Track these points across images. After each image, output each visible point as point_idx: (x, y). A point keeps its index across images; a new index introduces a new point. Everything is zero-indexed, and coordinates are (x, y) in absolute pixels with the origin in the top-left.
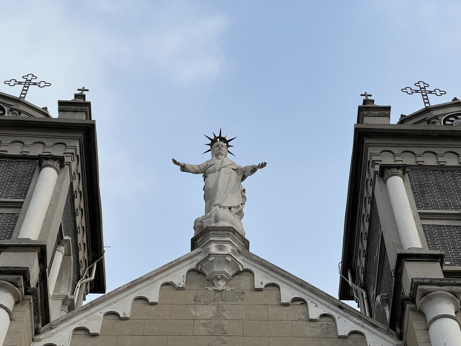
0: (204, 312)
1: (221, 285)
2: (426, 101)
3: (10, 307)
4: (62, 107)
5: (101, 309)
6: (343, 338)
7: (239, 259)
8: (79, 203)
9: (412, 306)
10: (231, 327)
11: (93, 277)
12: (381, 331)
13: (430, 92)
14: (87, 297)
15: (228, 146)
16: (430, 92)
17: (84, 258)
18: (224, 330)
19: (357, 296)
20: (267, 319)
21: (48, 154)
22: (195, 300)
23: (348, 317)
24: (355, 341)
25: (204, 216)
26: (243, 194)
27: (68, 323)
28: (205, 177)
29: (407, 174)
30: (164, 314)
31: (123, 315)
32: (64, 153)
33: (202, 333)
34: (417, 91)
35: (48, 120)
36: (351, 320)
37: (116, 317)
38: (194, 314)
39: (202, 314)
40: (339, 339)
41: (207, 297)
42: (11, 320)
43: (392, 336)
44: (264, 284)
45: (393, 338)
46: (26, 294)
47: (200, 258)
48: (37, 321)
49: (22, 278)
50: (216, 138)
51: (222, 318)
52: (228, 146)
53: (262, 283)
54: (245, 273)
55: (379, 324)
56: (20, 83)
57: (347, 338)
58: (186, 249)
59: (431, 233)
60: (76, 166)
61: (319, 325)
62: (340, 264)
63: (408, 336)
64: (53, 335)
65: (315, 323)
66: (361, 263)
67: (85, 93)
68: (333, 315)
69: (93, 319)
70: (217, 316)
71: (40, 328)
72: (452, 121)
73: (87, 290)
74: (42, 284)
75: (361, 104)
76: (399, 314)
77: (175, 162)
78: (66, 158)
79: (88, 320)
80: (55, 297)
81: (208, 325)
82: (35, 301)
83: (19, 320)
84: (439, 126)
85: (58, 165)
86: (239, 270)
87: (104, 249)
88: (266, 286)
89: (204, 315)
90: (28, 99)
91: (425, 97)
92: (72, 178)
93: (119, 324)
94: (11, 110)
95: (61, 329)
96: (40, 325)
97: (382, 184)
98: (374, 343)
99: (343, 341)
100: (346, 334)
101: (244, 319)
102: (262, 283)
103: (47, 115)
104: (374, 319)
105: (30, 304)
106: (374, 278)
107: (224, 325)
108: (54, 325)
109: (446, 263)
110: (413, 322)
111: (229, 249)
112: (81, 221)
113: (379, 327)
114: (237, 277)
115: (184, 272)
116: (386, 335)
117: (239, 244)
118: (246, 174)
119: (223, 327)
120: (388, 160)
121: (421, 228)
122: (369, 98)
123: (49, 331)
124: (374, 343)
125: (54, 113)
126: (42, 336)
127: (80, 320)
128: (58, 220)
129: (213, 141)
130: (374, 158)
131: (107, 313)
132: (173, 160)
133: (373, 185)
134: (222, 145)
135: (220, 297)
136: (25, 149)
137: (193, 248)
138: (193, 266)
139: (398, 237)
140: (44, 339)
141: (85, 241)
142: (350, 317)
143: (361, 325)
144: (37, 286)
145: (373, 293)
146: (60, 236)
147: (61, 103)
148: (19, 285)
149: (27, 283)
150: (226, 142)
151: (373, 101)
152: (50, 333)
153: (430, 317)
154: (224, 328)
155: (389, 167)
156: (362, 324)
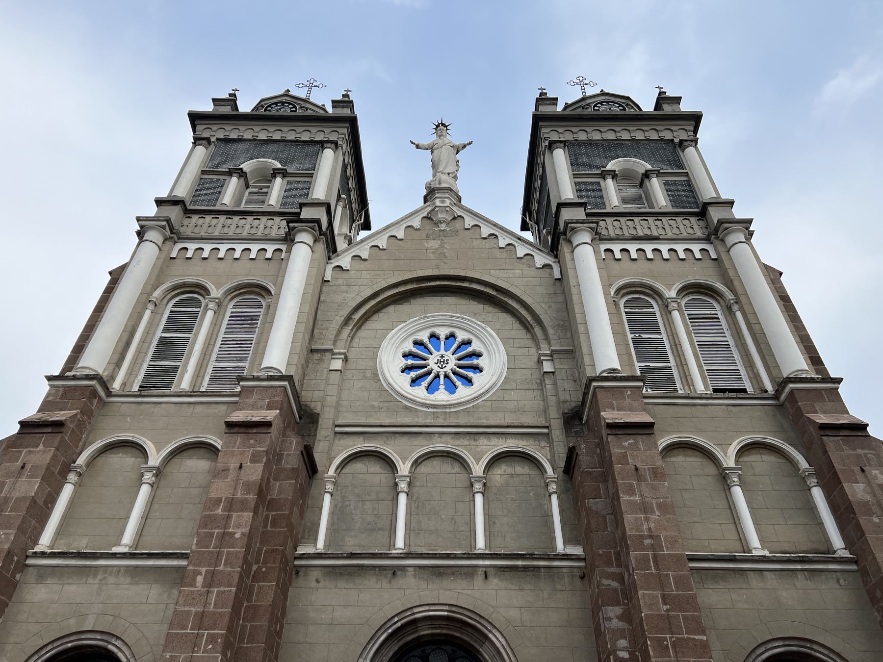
1: (443, 227)
2: (583, 91)
3: (311, 244)
4: (335, 104)
5: (368, 243)
7: (455, 209)
9: (564, 237)
11: (362, 221)
13: (586, 84)
14: (359, 233)
15: (447, 129)
16: (586, 84)
17: (356, 208)
19: (532, 229)
21: (327, 139)
22: (426, 237)
25: (432, 180)
26: (457, 163)
28: (432, 152)
29: (566, 147)
32: (338, 138)
34: (577, 84)
35: (326, 115)
37: (377, 248)
41: (434, 235)
43: (551, 256)
44: (471, 226)
46: (320, 235)
47: (429, 209)
48: (329, 252)
49: (317, 224)
50: (439, 124)
52: (447, 129)
53: (469, 225)
54: (458, 218)
55: (543, 249)
56: (306, 86)
58: (421, 203)
59: (580, 187)
60: (345, 147)
62: (522, 208)
63: (560, 256)
66: (535, 207)
67: (349, 93)
70: (441, 246)
72: (599, 107)
73: (359, 228)
74: (330, 228)
75: (538, 96)
76: (556, 242)
77: (412, 142)
78: (339, 141)
79: (361, 250)
80: (339, 235)
82: (327, 240)
84: (590, 111)
85: (334, 147)
86: (455, 216)
87: (369, 202)
88: (472, 227)
91: (583, 88)
92: (344, 155)
94: (301, 108)
96: (331, 254)
97: (550, 154)
102: (469, 225)
105: (323, 241)
106: (543, 218)
107: (445, 253)
109: (588, 207)
111: (448, 202)
112: (352, 184)
114: (453, 221)
115: (419, 218)
117: (454, 198)
118: (459, 149)
120: (554, 137)
121: (574, 184)
122: (544, 91)
125: (330, 110)
126: (332, 261)
128: (337, 185)
129: (437, 126)
130: (545, 136)
132: (410, 141)
134: (443, 129)
135: (443, 235)
137: (425, 202)
138: (425, 214)
139: (559, 191)
141: (356, 197)
144: (327, 230)
145: (542, 227)
147: (333, 102)
148: (315, 229)
150: (446, 126)
151: (546, 94)
153: (575, 244)
154: (446, 254)
155: (555, 142)
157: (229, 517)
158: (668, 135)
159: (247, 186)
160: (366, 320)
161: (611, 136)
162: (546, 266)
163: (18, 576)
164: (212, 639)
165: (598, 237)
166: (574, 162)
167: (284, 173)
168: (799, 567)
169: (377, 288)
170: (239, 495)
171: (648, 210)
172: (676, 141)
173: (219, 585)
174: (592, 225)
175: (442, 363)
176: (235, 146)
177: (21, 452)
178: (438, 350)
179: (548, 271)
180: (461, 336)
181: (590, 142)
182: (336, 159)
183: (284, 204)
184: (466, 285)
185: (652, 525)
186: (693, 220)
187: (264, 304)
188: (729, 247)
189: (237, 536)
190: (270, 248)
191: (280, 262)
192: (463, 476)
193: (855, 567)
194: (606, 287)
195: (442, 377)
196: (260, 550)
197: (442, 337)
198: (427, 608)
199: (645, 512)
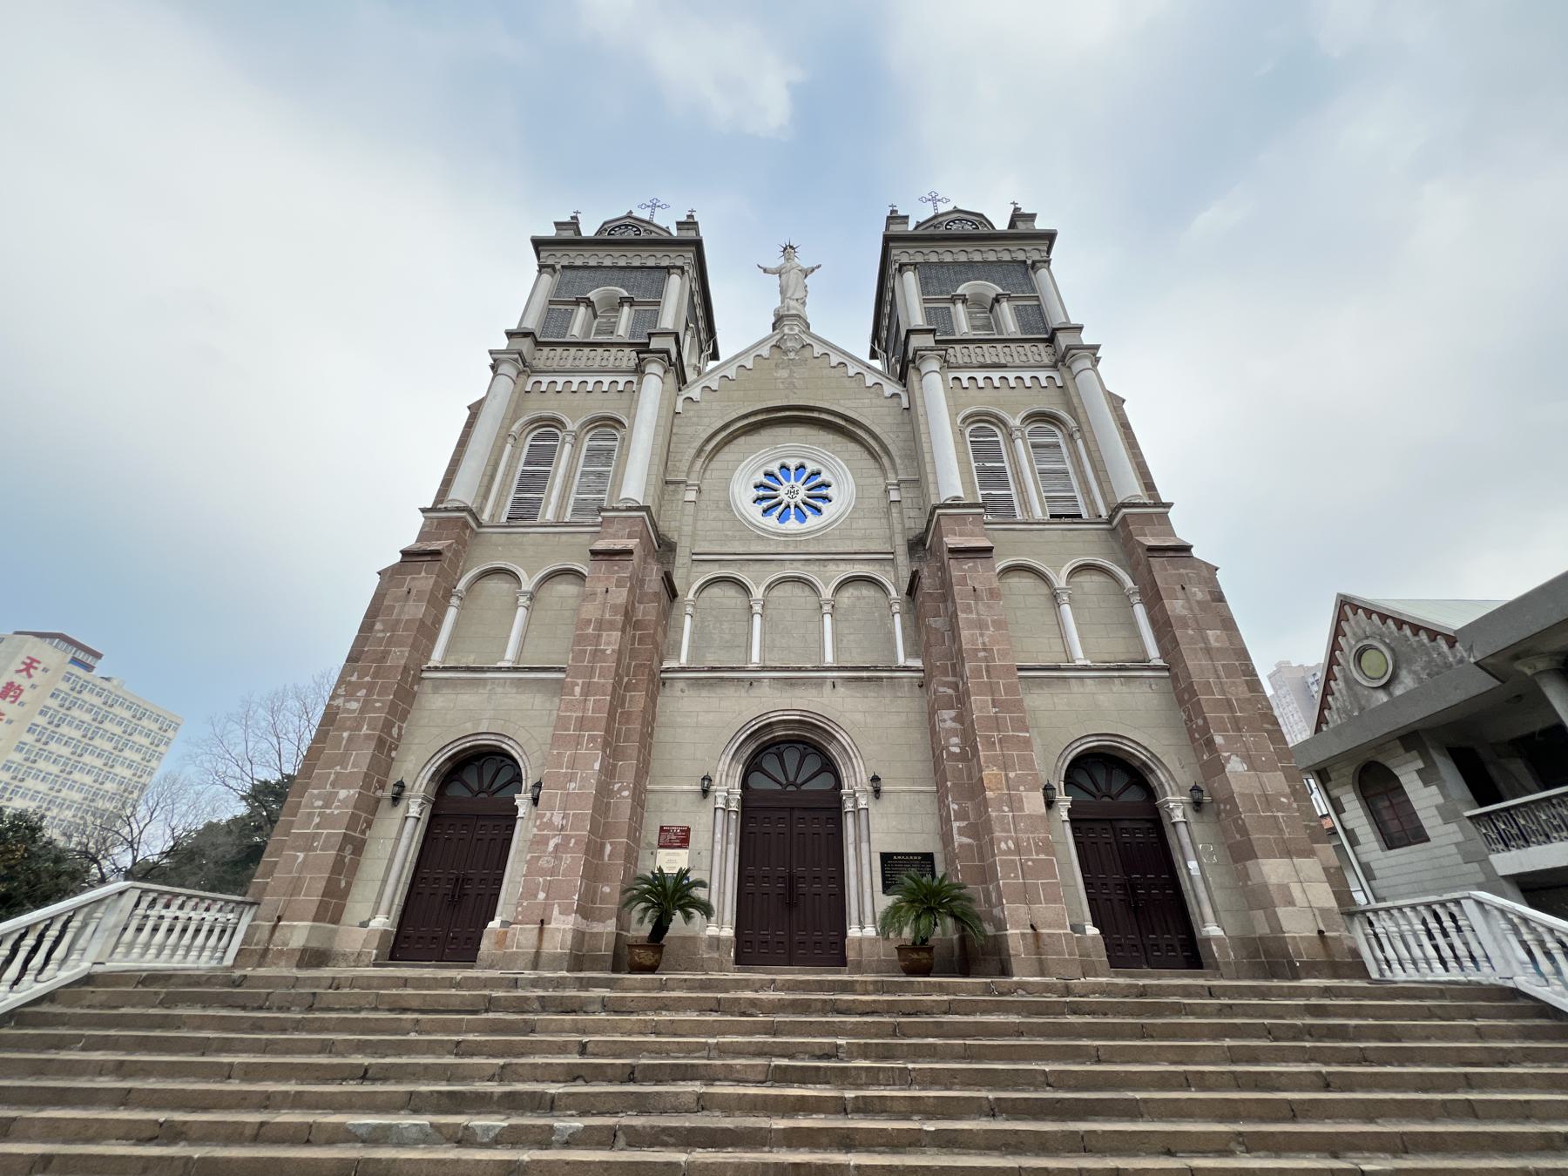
1: (792, 355)
7: (803, 336)
8: (697, 299)
28: (780, 276)
35: (992, 231)
47: (778, 337)
60: (692, 272)
63: (908, 385)
70: (790, 376)
84: (942, 230)
90: (656, 221)
92: (691, 281)
103: (670, 234)
111: (797, 330)
112: (700, 312)
120: (905, 259)
128: (684, 313)
133: (894, 279)
136: (644, 261)
137: (774, 330)
138: (774, 343)
145: (890, 355)
146: (687, 325)
147: (678, 223)
149: (670, 359)
150: (794, 249)
155: (906, 265)
157: (599, 636)
158: (1021, 256)
159: (595, 316)
160: (718, 451)
161: (963, 258)
162: (894, 395)
163: (416, 687)
164: (592, 739)
165: (947, 365)
166: (924, 285)
167: (631, 302)
168: (1116, 674)
169: (727, 419)
170: (607, 616)
171: (996, 337)
172: (1029, 262)
173: (595, 695)
174: (940, 352)
176: (580, 273)
177: (405, 579)
178: (788, 480)
179: (896, 400)
180: (811, 467)
181: (941, 264)
182: (683, 285)
183: (633, 335)
184: (815, 415)
185: (987, 640)
186: (1041, 346)
187: (618, 437)
188: (1075, 372)
189: (608, 652)
190: (622, 380)
191: (631, 395)
192: (813, 599)
193: (1167, 674)
194: (953, 416)
195: (792, 507)
196: (629, 665)
197: (792, 468)
198: (781, 713)
199: (981, 629)
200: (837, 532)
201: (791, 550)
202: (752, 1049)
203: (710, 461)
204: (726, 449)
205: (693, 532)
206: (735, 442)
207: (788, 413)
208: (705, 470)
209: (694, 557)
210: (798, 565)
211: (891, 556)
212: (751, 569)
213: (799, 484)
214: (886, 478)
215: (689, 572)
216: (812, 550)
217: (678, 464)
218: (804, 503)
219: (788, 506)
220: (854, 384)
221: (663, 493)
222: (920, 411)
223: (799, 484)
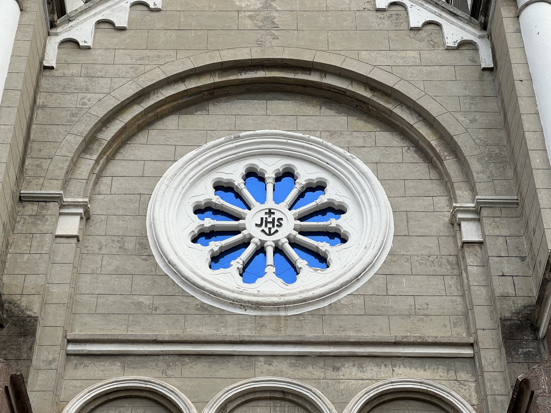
0: (251, 2)
6: (416, 30)
10: (282, 19)
12: (461, 20)
18: (275, 24)
20: (325, 9)
23: (423, 5)
24: (430, 33)
27: (89, 15)
30: (203, 4)
31: (154, 5)
33: (249, 27)
36: (426, 9)
37: (145, 8)
38: (238, 4)
39: (247, 5)
40: (411, 31)
42: (21, 10)
43: (474, 26)
45: (474, 28)
48: (51, 12)
51: (272, 9)
55: (459, 13)
57: (420, 30)
61: (388, 15)
64: (72, 28)
65: (383, 13)
68: (404, 4)
69: (118, 10)
71: (56, 20)
79: (113, 11)
81: (256, 17)
83: (32, 10)
89: (250, 5)
93: (149, 16)
95: (81, 21)
96: (56, 17)
98: (453, 34)
99: (416, 34)
100: (420, 25)
101: (298, 10)
104: (451, 5)
107: (275, 18)
108: (72, 17)
110: (501, 9)
113: (460, 16)
116: (468, 25)
119: (274, 20)
123: (67, 24)
124: (453, 34)
126: (59, 30)
127: (102, 10)
131: (133, 4)
140: (63, 33)
142: (425, 4)
143: (438, 14)
152: (68, 26)
154: (275, 21)
156: (439, 13)
160: (124, 143)
162: (464, 44)
175: (270, 225)
178: (262, 200)
179: (467, 53)
184: (314, 78)
195: (270, 251)
197: (270, 175)
200: (359, 301)
201: (268, 334)
202: (238, 158)
203: (108, 161)
204: (141, 138)
205: (71, 297)
206: (160, 125)
207: (261, 74)
208: (99, 177)
209: (72, 348)
210: (283, 365)
211: (468, 352)
212: (186, 373)
213: (283, 206)
214: (452, 197)
215: (60, 377)
216: (310, 335)
217: (45, 164)
218: (294, 244)
219: (261, 250)
220: (387, 24)
221: (13, 218)
222: (518, 72)
223: (283, 206)
